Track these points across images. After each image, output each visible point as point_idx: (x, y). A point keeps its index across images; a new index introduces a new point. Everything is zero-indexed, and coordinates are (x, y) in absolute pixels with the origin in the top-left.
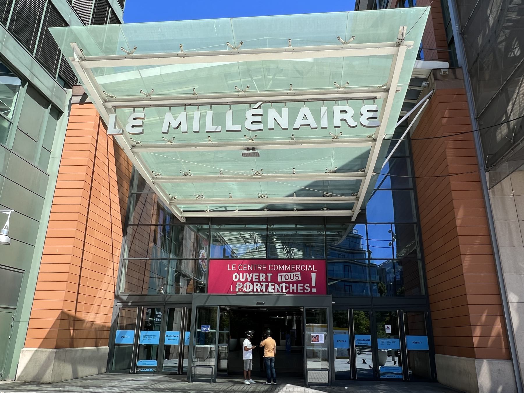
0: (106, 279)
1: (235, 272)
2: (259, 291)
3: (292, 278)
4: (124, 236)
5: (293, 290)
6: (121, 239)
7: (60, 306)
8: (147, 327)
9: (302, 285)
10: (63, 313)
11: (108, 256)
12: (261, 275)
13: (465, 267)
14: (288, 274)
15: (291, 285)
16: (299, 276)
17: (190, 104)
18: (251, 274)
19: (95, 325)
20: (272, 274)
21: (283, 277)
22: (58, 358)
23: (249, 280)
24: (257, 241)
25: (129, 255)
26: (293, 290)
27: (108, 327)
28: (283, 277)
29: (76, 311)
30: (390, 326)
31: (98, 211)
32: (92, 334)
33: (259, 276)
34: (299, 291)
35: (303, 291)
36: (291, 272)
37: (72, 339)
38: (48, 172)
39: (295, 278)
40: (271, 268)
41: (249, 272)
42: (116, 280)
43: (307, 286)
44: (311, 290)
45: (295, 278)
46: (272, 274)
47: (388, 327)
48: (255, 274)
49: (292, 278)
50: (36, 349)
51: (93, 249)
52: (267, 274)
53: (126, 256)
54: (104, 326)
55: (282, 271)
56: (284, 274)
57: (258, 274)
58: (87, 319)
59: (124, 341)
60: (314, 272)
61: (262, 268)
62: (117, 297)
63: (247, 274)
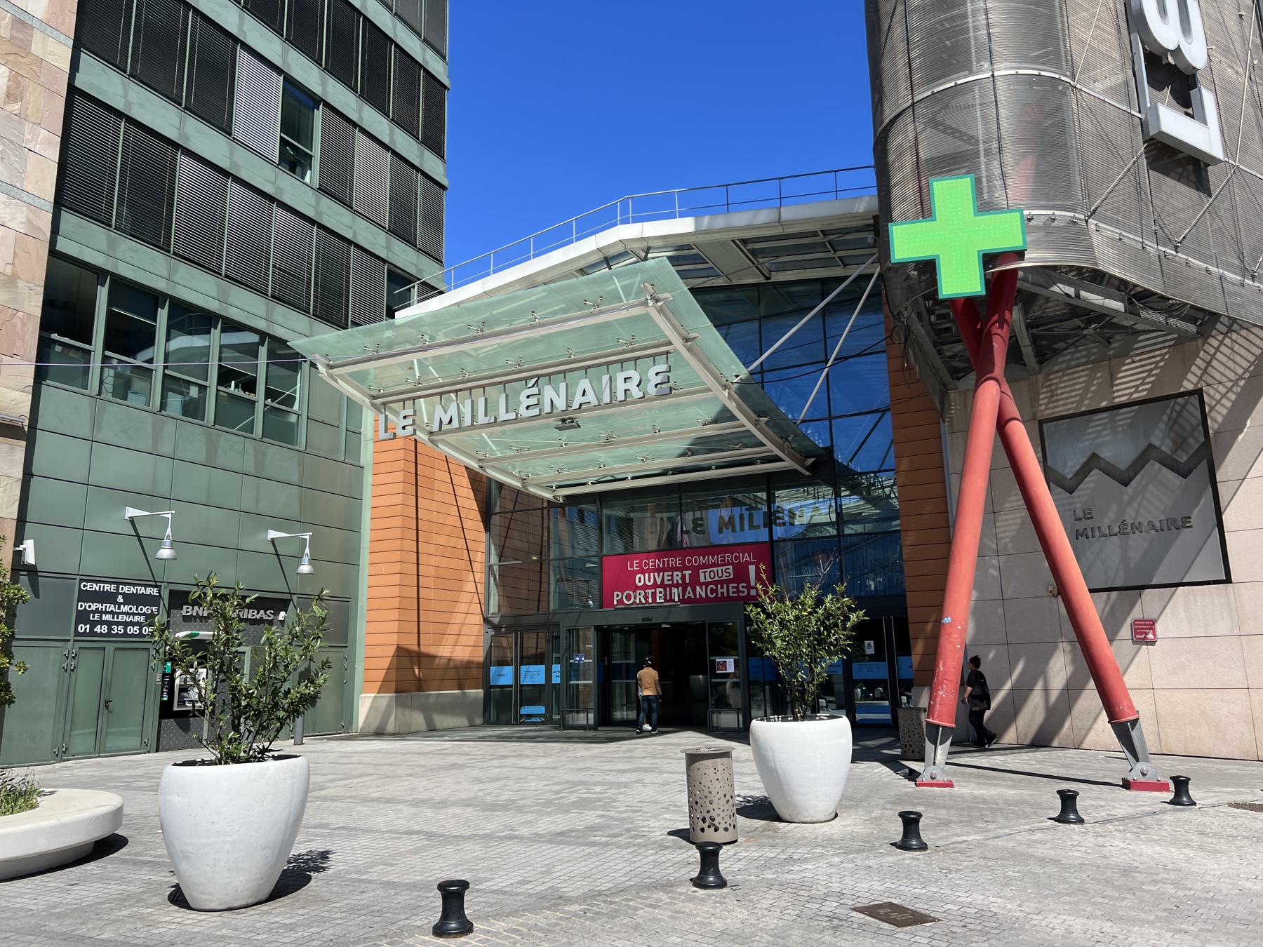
0: (465, 597)
1: (637, 572)
2: (644, 601)
3: (720, 575)
4: (486, 531)
5: (722, 593)
6: (483, 536)
7: (394, 639)
8: (537, 659)
9: (736, 585)
10: (399, 648)
11: (463, 565)
12: (675, 573)
13: (906, 550)
14: (715, 569)
15: (719, 586)
16: (731, 571)
17: (461, 390)
18: (661, 574)
19: (454, 660)
20: (690, 572)
21: (707, 574)
22: (400, 704)
23: (659, 583)
24: (1236, 383)
25: (501, 557)
26: (722, 593)
27: (478, 663)
28: (707, 574)
29: (419, 645)
30: (872, 643)
31: (434, 506)
32: (452, 673)
33: (672, 576)
34: (731, 595)
35: (736, 595)
36: (719, 565)
37: (419, 680)
38: (361, 464)
39: (725, 574)
40: (690, 561)
41: (658, 570)
42: (482, 597)
43: (743, 587)
44: (749, 592)
45: (725, 574)
46: (690, 572)
47: (869, 644)
48: (666, 574)
49: (720, 575)
50: (374, 695)
51: (435, 561)
52: (684, 572)
53: (494, 559)
54: (469, 663)
55: (705, 566)
56: (709, 570)
57: (670, 573)
58: (440, 654)
59: (502, 682)
60: (752, 563)
61: (676, 563)
62: (486, 620)
63: (656, 574)
